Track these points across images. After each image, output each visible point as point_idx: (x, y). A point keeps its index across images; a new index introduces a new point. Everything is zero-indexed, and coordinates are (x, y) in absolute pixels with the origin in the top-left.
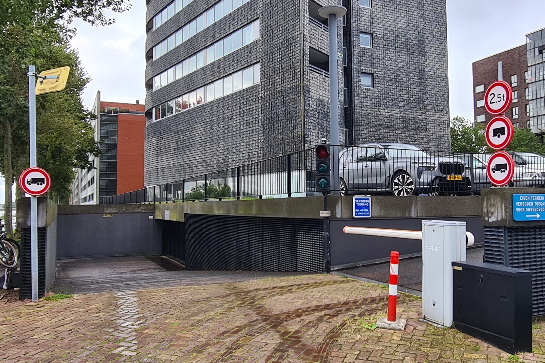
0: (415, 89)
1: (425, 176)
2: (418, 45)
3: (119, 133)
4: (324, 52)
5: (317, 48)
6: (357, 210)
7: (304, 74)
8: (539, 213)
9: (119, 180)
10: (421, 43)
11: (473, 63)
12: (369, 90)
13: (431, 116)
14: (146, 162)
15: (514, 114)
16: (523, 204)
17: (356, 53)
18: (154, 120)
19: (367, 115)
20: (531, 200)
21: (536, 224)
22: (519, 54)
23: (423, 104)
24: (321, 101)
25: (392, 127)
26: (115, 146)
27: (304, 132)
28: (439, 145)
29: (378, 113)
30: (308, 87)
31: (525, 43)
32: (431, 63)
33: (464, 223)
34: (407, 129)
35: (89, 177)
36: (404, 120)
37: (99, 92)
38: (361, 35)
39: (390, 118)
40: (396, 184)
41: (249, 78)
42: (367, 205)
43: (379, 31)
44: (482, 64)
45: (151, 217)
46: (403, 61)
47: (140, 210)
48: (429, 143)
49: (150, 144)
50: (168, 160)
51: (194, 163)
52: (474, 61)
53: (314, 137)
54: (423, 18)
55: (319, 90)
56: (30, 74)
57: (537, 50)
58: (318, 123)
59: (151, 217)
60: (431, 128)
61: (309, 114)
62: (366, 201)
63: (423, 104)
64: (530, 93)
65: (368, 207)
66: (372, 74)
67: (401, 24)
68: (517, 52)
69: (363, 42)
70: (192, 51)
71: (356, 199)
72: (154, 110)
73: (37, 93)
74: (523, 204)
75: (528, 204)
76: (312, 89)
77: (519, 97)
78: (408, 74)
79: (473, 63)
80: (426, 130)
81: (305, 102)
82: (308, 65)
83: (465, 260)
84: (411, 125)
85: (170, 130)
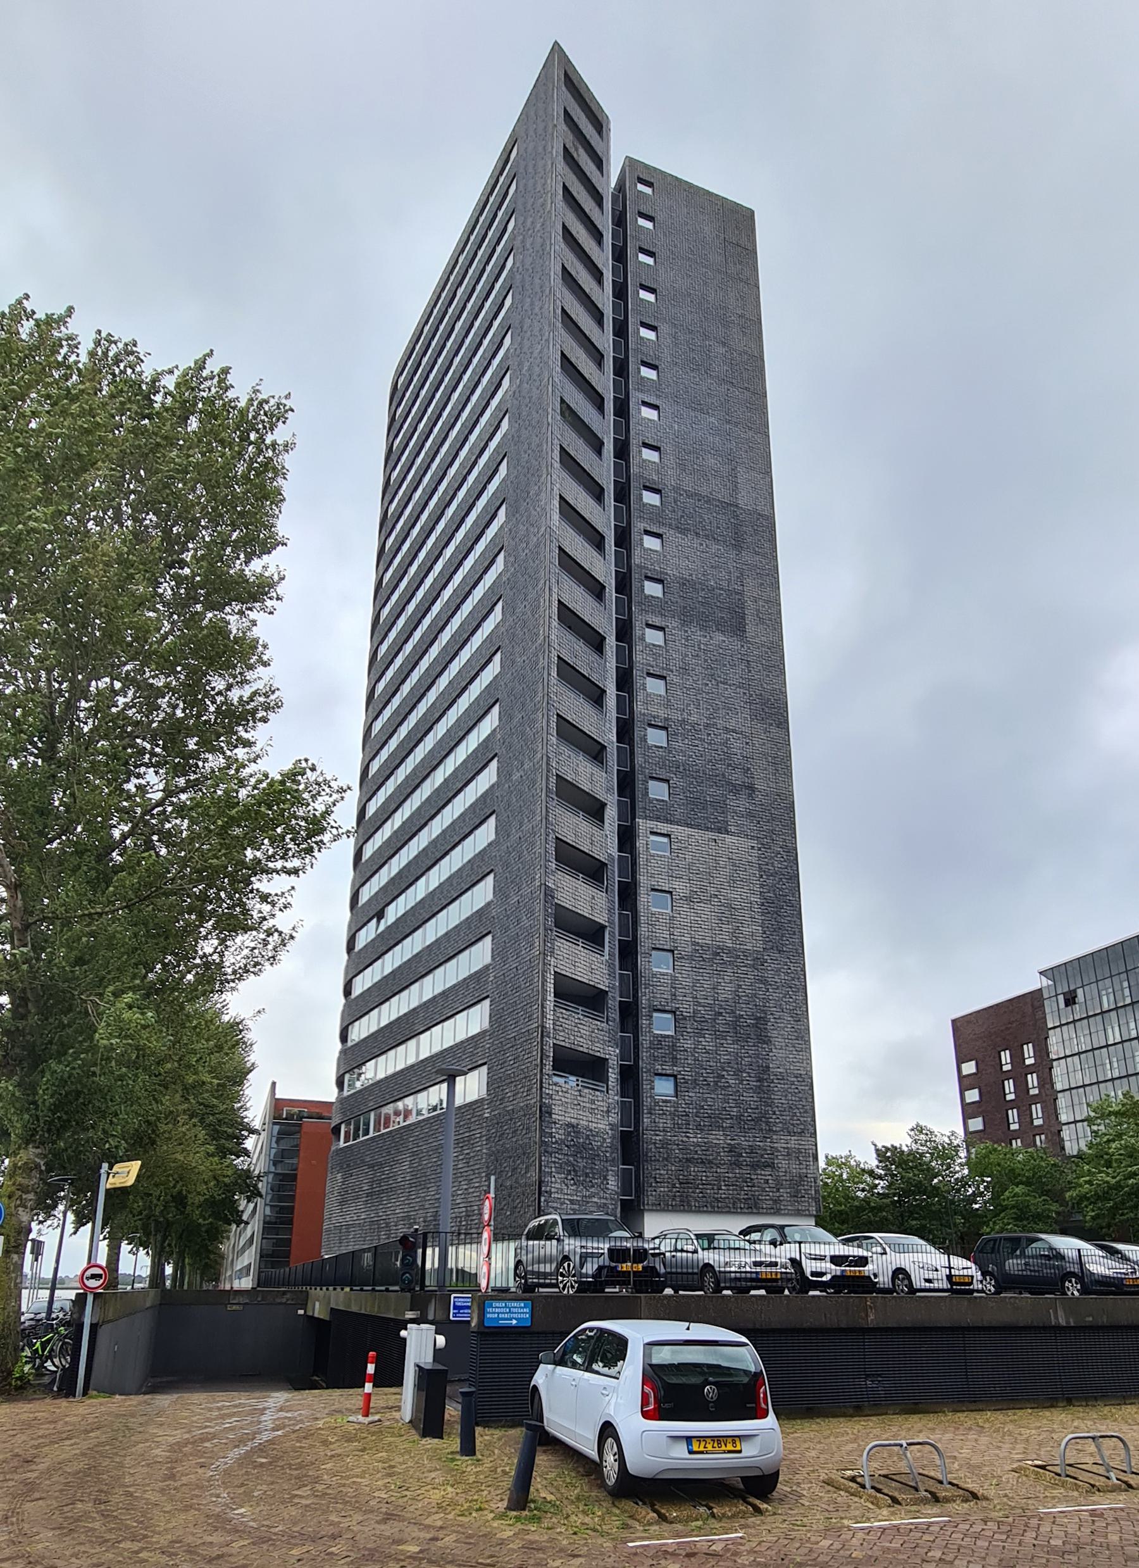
1: (589, 1265)
2: (755, 1026)
3: (302, 1154)
4: (581, 1049)
5: (567, 1045)
7: (541, 1087)
9: (295, 1239)
10: (760, 1022)
11: (954, 1021)
12: (669, 1101)
13: (782, 1142)
14: (326, 1215)
15: (1034, 1116)
17: (646, 1044)
18: (342, 1144)
19: (665, 1144)
20: (506, 1307)
22: (1032, 1005)
23: (767, 1123)
24: (573, 1126)
25: (710, 1162)
26: (294, 1178)
27: (540, 1177)
28: (798, 1191)
29: (685, 1139)
30: (550, 1106)
31: (1038, 986)
33: (434, 1327)
34: (738, 1165)
35: (249, 1233)
36: (732, 1149)
37: (274, 1084)
38: (655, 1015)
39: (708, 1146)
40: (562, 1275)
41: (471, 1087)
43: (686, 1008)
44: (969, 1022)
45: (301, 1312)
46: (729, 1054)
47: (284, 1300)
48: (778, 1190)
49: (334, 1181)
50: (357, 1213)
51: (393, 1220)
53: (557, 1186)
54: (763, 981)
55: (569, 1110)
56: (102, 1171)
57: (1061, 998)
58: (568, 1163)
59: (301, 1312)
61: (550, 1149)
63: (767, 1123)
64: (1060, 1078)
66: (675, 1076)
67: (726, 992)
68: (1028, 1000)
69: (662, 1025)
70: (400, 1038)
72: (343, 1126)
73: (108, 1186)
75: (502, 1310)
76: (556, 1109)
77: (1041, 1086)
78: (738, 1073)
79: (954, 1021)
80: (772, 1166)
81: (541, 1130)
82: (551, 1073)
84: (745, 1158)
85: (363, 1161)
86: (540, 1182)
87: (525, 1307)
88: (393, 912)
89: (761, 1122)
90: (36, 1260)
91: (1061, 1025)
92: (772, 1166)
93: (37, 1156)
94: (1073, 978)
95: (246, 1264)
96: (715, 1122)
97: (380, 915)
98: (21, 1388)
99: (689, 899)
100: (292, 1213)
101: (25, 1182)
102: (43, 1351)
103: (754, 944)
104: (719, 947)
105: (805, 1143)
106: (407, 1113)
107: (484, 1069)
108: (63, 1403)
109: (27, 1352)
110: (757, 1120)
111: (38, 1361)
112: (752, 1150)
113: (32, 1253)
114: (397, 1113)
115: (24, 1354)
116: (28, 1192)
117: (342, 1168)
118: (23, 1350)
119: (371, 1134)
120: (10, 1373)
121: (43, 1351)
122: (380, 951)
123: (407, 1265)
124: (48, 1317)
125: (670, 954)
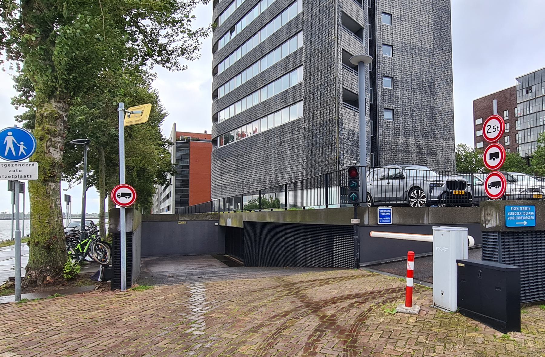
0: (427, 122)
1: (435, 191)
2: (430, 86)
4: (354, 92)
5: (349, 89)
6: (381, 219)
8: (526, 220)
10: (432, 85)
11: (474, 101)
12: (391, 122)
13: (440, 143)
16: (514, 213)
18: (219, 147)
19: (389, 143)
20: (519, 211)
21: (523, 230)
23: (434, 134)
24: (352, 131)
25: (409, 152)
26: (188, 167)
27: (339, 156)
28: (446, 166)
30: (342, 120)
31: (515, 85)
32: (440, 101)
33: (466, 229)
36: (418, 146)
37: (175, 124)
38: (384, 78)
41: (295, 113)
42: (389, 214)
43: (398, 76)
44: (481, 102)
45: (216, 224)
47: (207, 219)
49: (215, 165)
50: (230, 178)
51: (251, 181)
52: (474, 99)
54: (434, 64)
55: (350, 123)
57: (524, 90)
58: (350, 149)
59: (216, 224)
60: (440, 152)
62: (388, 211)
63: (434, 134)
65: (389, 216)
66: (393, 110)
68: (509, 92)
69: (386, 84)
70: (249, 92)
71: (380, 210)
74: (514, 213)
75: (518, 213)
76: (345, 122)
77: (510, 128)
78: (421, 109)
79: (474, 101)
80: (435, 154)
81: (339, 132)
82: (342, 102)
83: (467, 258)
85: (231, 154)
86: (339, 158)
87: (531, 211)
88: (239, 28)
89: (431, 133)
90: (68, 204)
91: (523, 102)
92: (435, 154)
93: (60, 108)
94: (529, 83)
95: (167, 205)
96: (411, 132)
97: (232, 30)
98: (72, 279)
99: (400, 20)
100: (189, 183)
101: (53, 128)
102: (83, 250)
103: (429, 45)
104: (413, 46)
105: (450, 144)
106: (243, 135)
107: (302, 103)
108: (112, 295)
109: (72, 251)
110: (429, 132)
111: (80, 257)
112: (427, 147)
113: (66, 201)
114: (239, 135)
115: (69, 253)
116: (56, 136)
117: (220, 158)
118: (68, 250)
119: (235, 141)
120: (61, 269)
121: (83, 250)
122: (234, 48)
123: (353, 187)
124: (83, 229)
125: (390, 48)
